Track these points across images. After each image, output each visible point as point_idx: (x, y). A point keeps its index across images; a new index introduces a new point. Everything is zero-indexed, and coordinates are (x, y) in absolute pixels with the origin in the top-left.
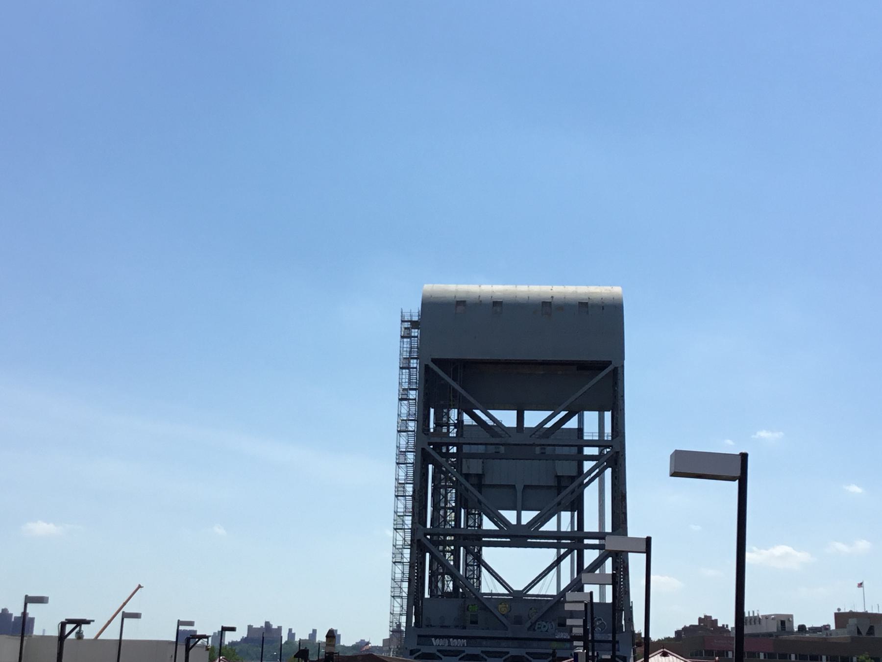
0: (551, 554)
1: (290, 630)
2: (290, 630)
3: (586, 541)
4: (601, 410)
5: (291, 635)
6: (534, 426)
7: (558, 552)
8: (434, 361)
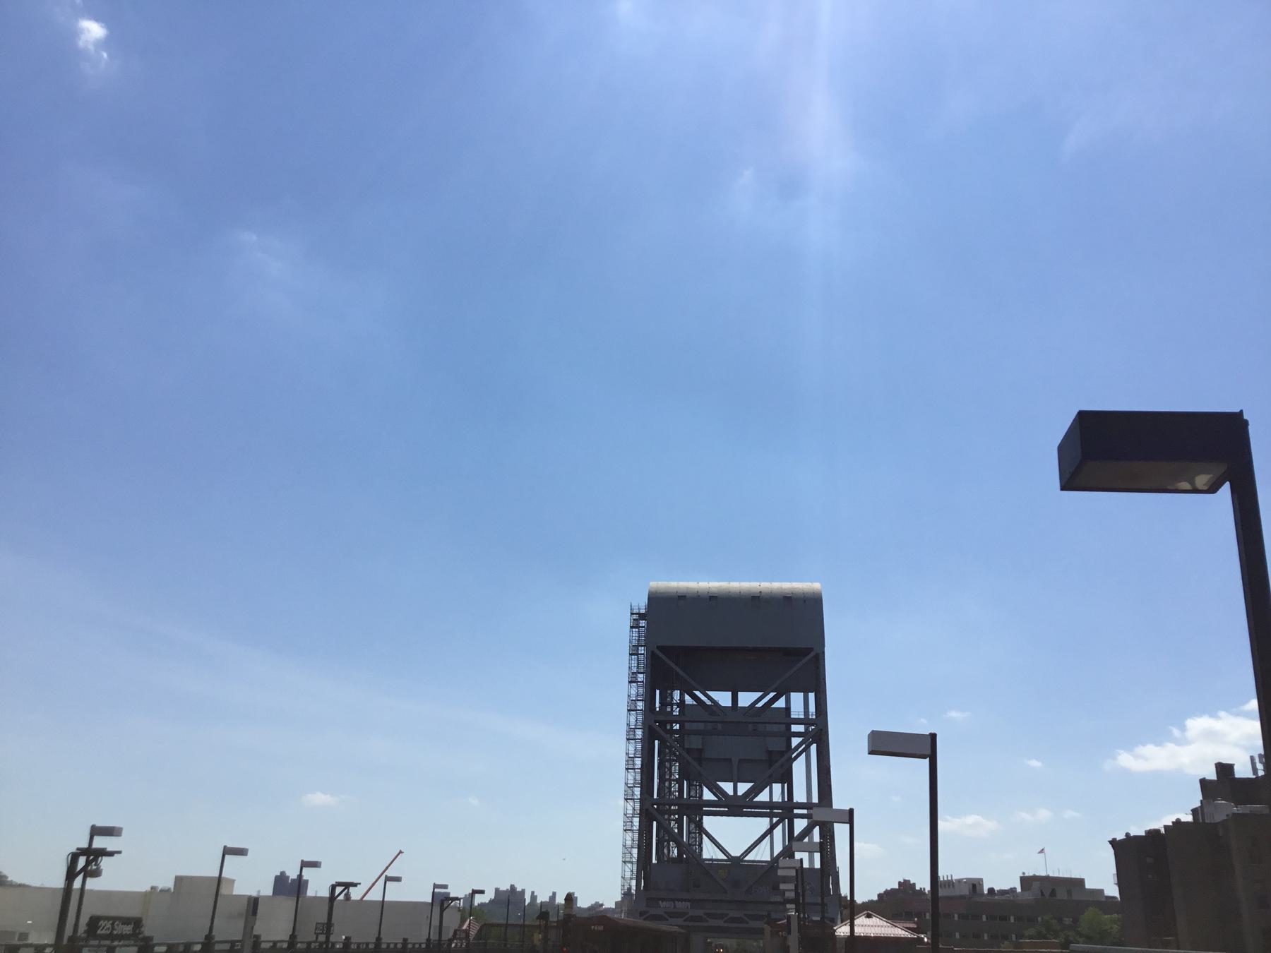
0: (764, 823)
1: (533, 893)
2: (533, 893)
3: (796, 811)
4: (806, 692)
5: (534, 897)
6: (747, 706)
7: (771, 821)
8: (660, 648)
